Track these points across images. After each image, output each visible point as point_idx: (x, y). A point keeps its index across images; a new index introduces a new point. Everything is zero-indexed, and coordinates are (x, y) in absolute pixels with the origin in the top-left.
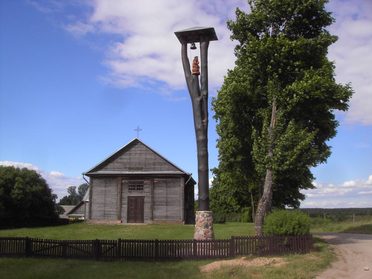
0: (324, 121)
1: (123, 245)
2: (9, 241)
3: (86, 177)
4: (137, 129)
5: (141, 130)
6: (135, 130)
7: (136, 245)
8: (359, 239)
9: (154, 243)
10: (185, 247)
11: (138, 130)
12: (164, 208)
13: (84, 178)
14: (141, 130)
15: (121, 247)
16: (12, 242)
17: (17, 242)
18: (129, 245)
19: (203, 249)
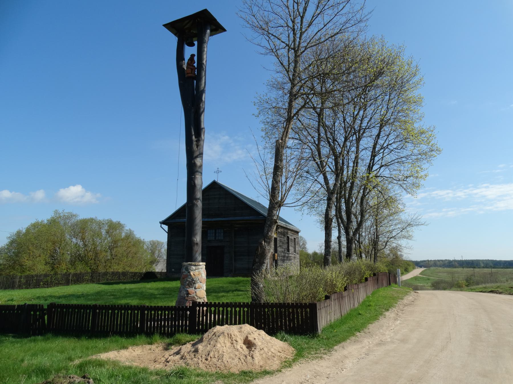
0: (363, 267)
1: (199, 310)
2: (181, 312)
3: (163, 226)
4: (217, 171)
5: (221, 172)
6: (215, 172)
7: (229, 312)
8: (100, 343)
9: (308, 310)
10: (213, 312)
11: (218, 172)
12: (333, 303)
13: (161, 227)
14: (221, 172)
15: (226, 315)
16: (121, 313)
17: (227, 311)
18: (225, 311)
19: (205, 317)
